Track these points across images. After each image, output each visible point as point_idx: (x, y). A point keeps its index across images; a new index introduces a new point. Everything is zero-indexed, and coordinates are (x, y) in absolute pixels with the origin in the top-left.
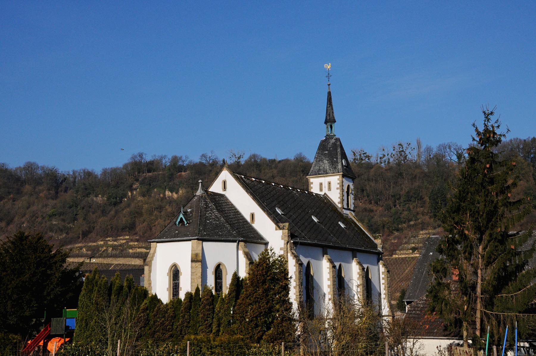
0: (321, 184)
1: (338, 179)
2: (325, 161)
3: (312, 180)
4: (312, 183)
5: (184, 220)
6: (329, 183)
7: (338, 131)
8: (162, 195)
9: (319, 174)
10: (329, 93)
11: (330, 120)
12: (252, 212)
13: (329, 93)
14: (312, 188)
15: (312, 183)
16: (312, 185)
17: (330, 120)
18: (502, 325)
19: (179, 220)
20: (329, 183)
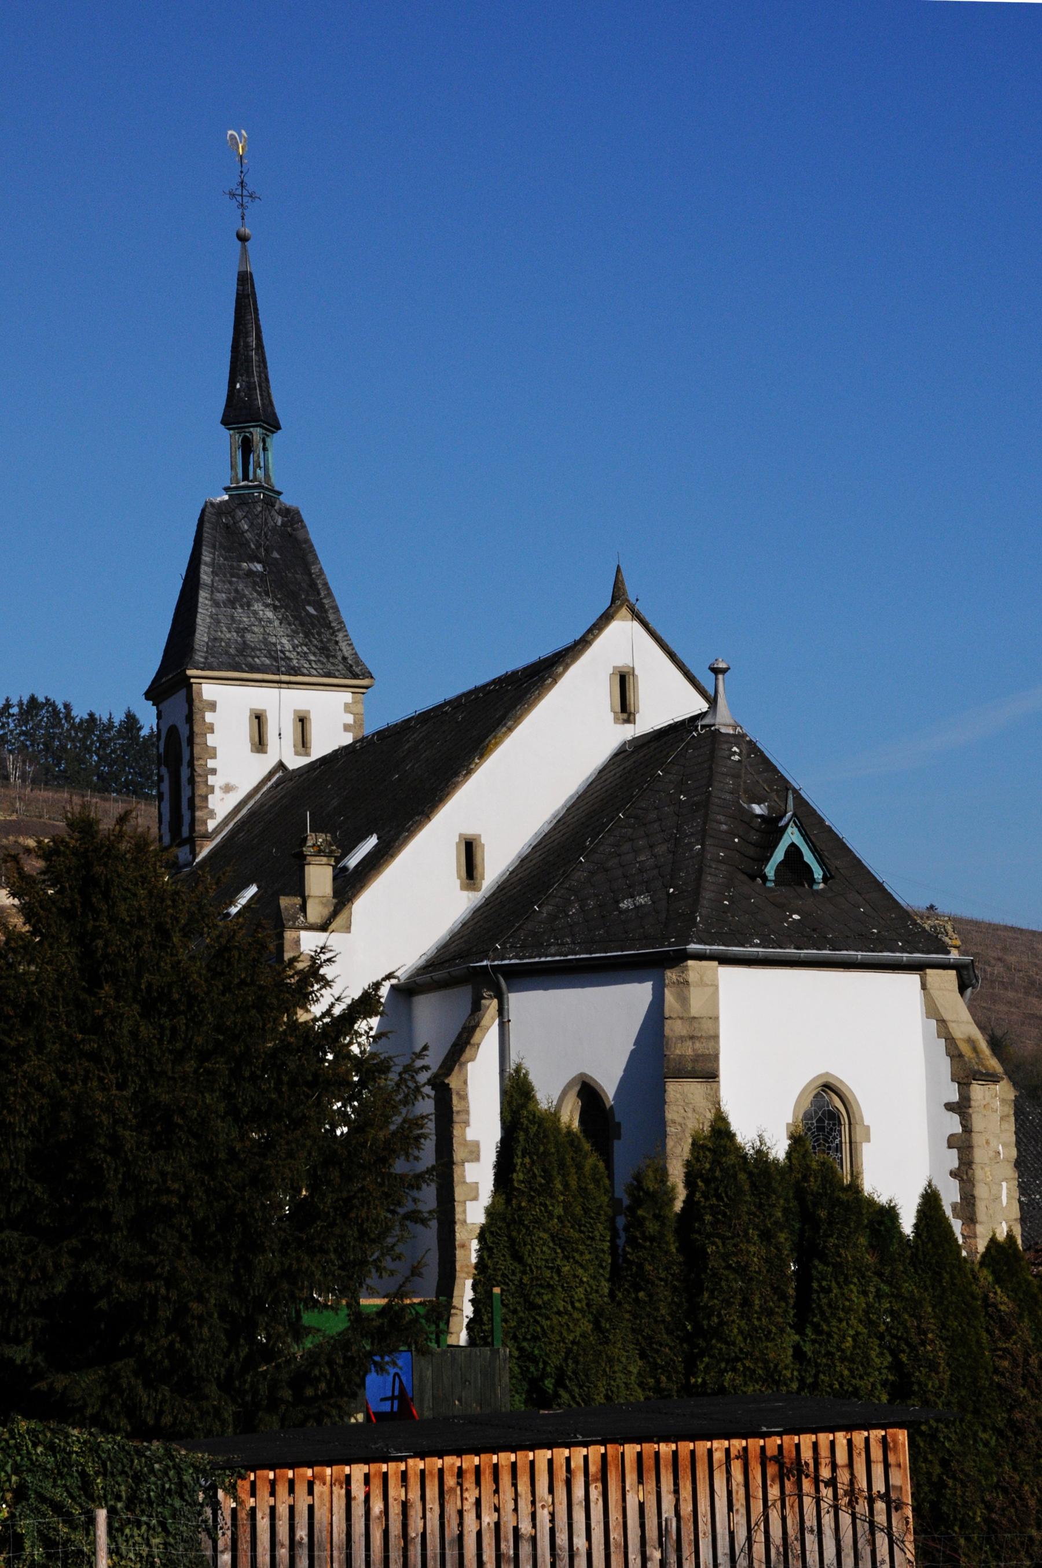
0: (259, 718)
1: (347, 708)
2: (257, 606)
3: (209, 691)
4: (212, 706)
5: (809, 857)
6: (302, 721)
7: (289, 467)
8: (223, 644)
9: (253, 669)
10: (245, 280)
11: (249, 411)
12: (470, 831)
13: (245, 280)
14: (211, 729)
15: (212, 706)
16: (209, 717)
17: (249, 411)
18: (593, 1469)
19: (779, 855)
20: (302, 721)
